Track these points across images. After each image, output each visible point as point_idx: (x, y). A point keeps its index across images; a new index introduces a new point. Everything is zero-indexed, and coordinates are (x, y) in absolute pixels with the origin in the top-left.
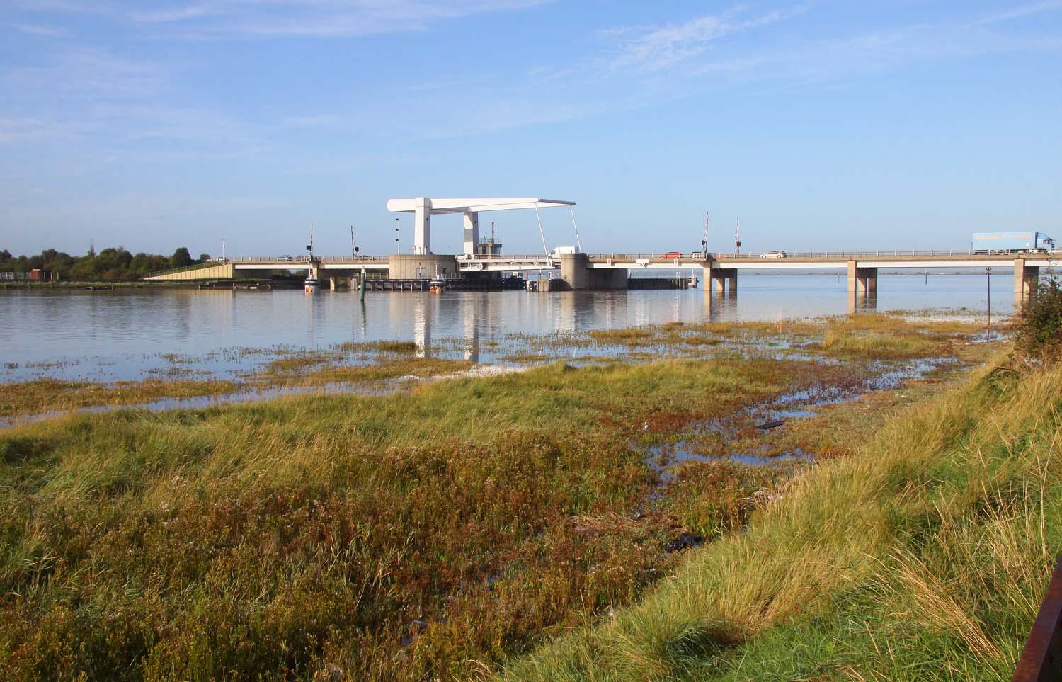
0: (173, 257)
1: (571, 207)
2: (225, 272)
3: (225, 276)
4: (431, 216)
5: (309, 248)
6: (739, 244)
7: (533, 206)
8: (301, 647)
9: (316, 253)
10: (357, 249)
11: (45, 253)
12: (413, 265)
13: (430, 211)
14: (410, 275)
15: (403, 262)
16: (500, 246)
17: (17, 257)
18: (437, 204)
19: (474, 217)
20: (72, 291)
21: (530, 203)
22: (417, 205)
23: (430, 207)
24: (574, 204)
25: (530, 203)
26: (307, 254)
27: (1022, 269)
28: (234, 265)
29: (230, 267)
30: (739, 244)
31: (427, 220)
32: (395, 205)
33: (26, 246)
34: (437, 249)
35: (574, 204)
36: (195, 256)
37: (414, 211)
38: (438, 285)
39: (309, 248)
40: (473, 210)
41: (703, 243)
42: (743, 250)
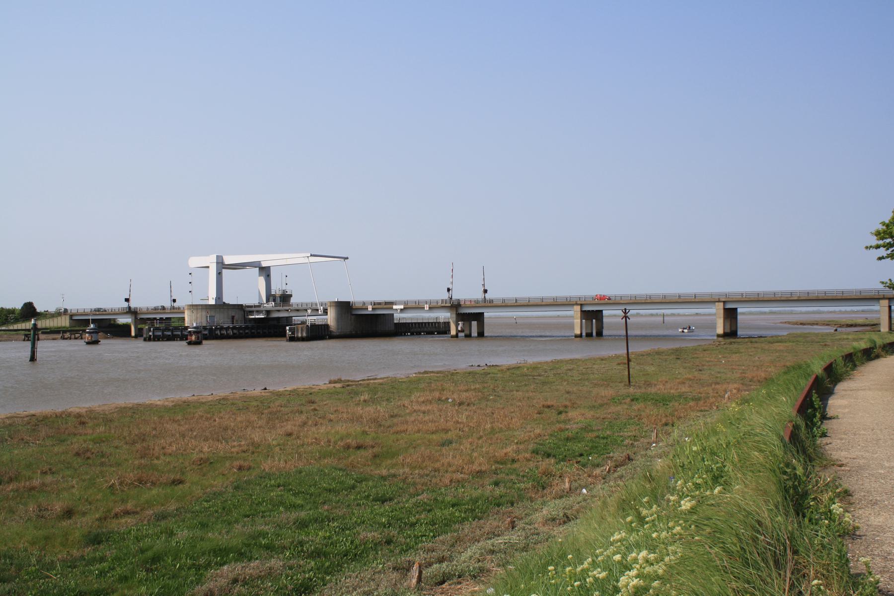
2: (64, 322)
3: (63, 325)
4: (224, 271)
5: (127, 300)
6: (485, 291)
7: (306, 260)
8: (307, 587)
9: (133, 304)
10: (174, 301)
13: (221, 266)
15: (195, 312)
18: (228, 260)
19: (265, 271)
20: (440, 304)
21: (299, 258)
22: (211, 261)
23: (222, 263)
24: (867, 248)
25: (299, 258)
26: (126, 305)
27: (722, 311)
28: (71, 316)
30: (485, 291)
31: (219, 274)
32: (195, 262)
35: (867, 248)
36: (39, 309)
37: (208, 267)
38: (194, 332)
39: (127, 300)
40: (264, 265)
41: (449, 290)
42: (488, 296)
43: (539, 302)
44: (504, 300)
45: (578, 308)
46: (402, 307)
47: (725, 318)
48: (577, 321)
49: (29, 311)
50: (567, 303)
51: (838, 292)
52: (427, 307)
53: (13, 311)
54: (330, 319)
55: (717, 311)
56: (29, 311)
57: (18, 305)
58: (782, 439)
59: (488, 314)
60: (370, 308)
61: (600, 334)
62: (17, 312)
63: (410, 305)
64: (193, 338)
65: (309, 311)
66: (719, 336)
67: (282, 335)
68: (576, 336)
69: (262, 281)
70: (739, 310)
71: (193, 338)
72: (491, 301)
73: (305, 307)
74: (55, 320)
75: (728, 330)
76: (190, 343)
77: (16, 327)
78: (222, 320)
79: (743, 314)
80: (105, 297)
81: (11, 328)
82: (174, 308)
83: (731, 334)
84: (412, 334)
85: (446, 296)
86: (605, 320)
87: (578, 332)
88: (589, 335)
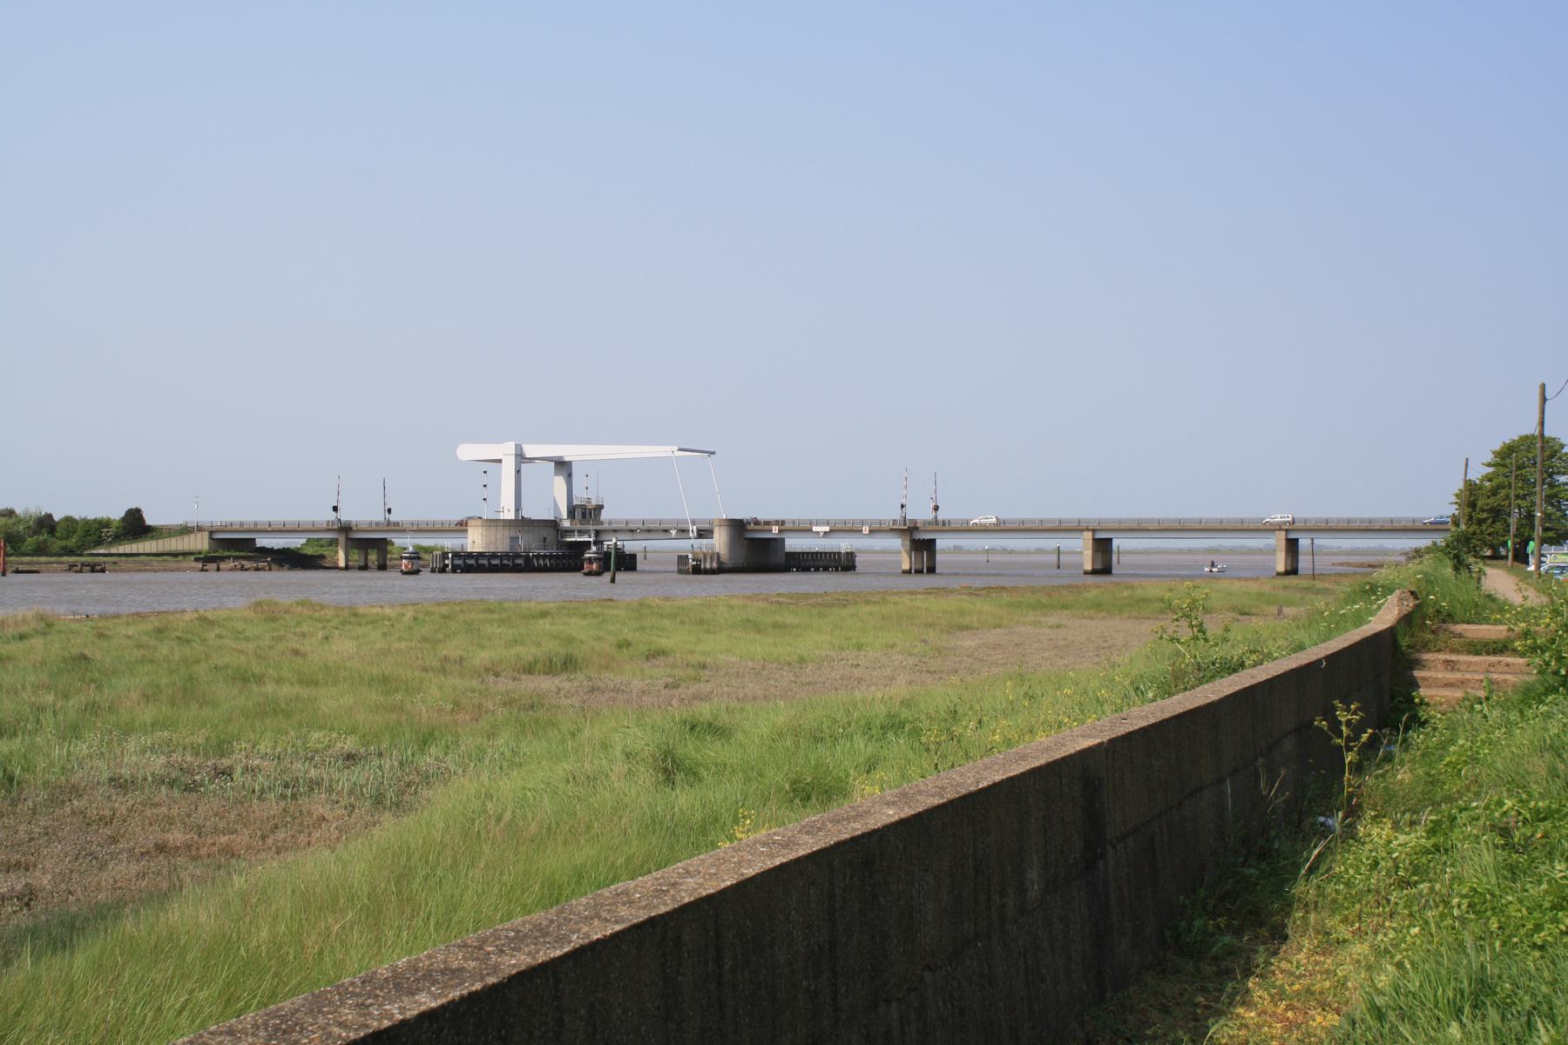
0: (123, 519)
1: (710, 460)
2: (201, 543)
6: (936, 508)
9: (346, 516)
11: (1506, 454)
12: (507, 533)
13: (521, 458)
14: (502, 546)
15: (493, 530)
16: (601, 507)
17: (1453, 510)
19: (562, 466)
22: (506, 451)
27: (1090, 544)
28: (211, 533)
29: (206, 535)
30: (936, 508)
32: (468, 452)
33: (29, 500)
34: (531, 512)
35: (1543, 387)
36: (150, 520)
37: (500, 461)
39: (335, 509)
43: (1218, 526)
44: (242, 524)
45: (1089, 535)
46: (827, 529)
47: (1095, 551)
48: (1089, 553)
49: (134, 525)
50: (1075, 529)
51: (1175, 520)
52: (866, 530)
53: (104, 524)
54: (719, 542)
55: (1278, 541)
56: (134, 525)
57: (117, 514)
58: (72, 954)
59: (942, 543)
60: (775, 529)
61: (932, 570)
62: (115, 525)
63: (838, 526)
64: (594, 566)
65: (674, 532)
66: (1086, 573)
67: (577, 568)
68: (904, 572)
69: (560, 483)
70: (1115, 543)
71: (594, 566)
72: (397, 524)
73: (664, 526)
74: (186, 538)
75: (1099, 566)
76: (590, 574)
77: (121, 549)
78: (527, 543)
79: (944, 551)
80: (285, 502)
81: (114, 551)
82: (389, 523)
83: (1104, 569)
84: (817, 570)
85: (897, 515)
86: (938, 558)
87: (906, 566)
88: (919, 572)
